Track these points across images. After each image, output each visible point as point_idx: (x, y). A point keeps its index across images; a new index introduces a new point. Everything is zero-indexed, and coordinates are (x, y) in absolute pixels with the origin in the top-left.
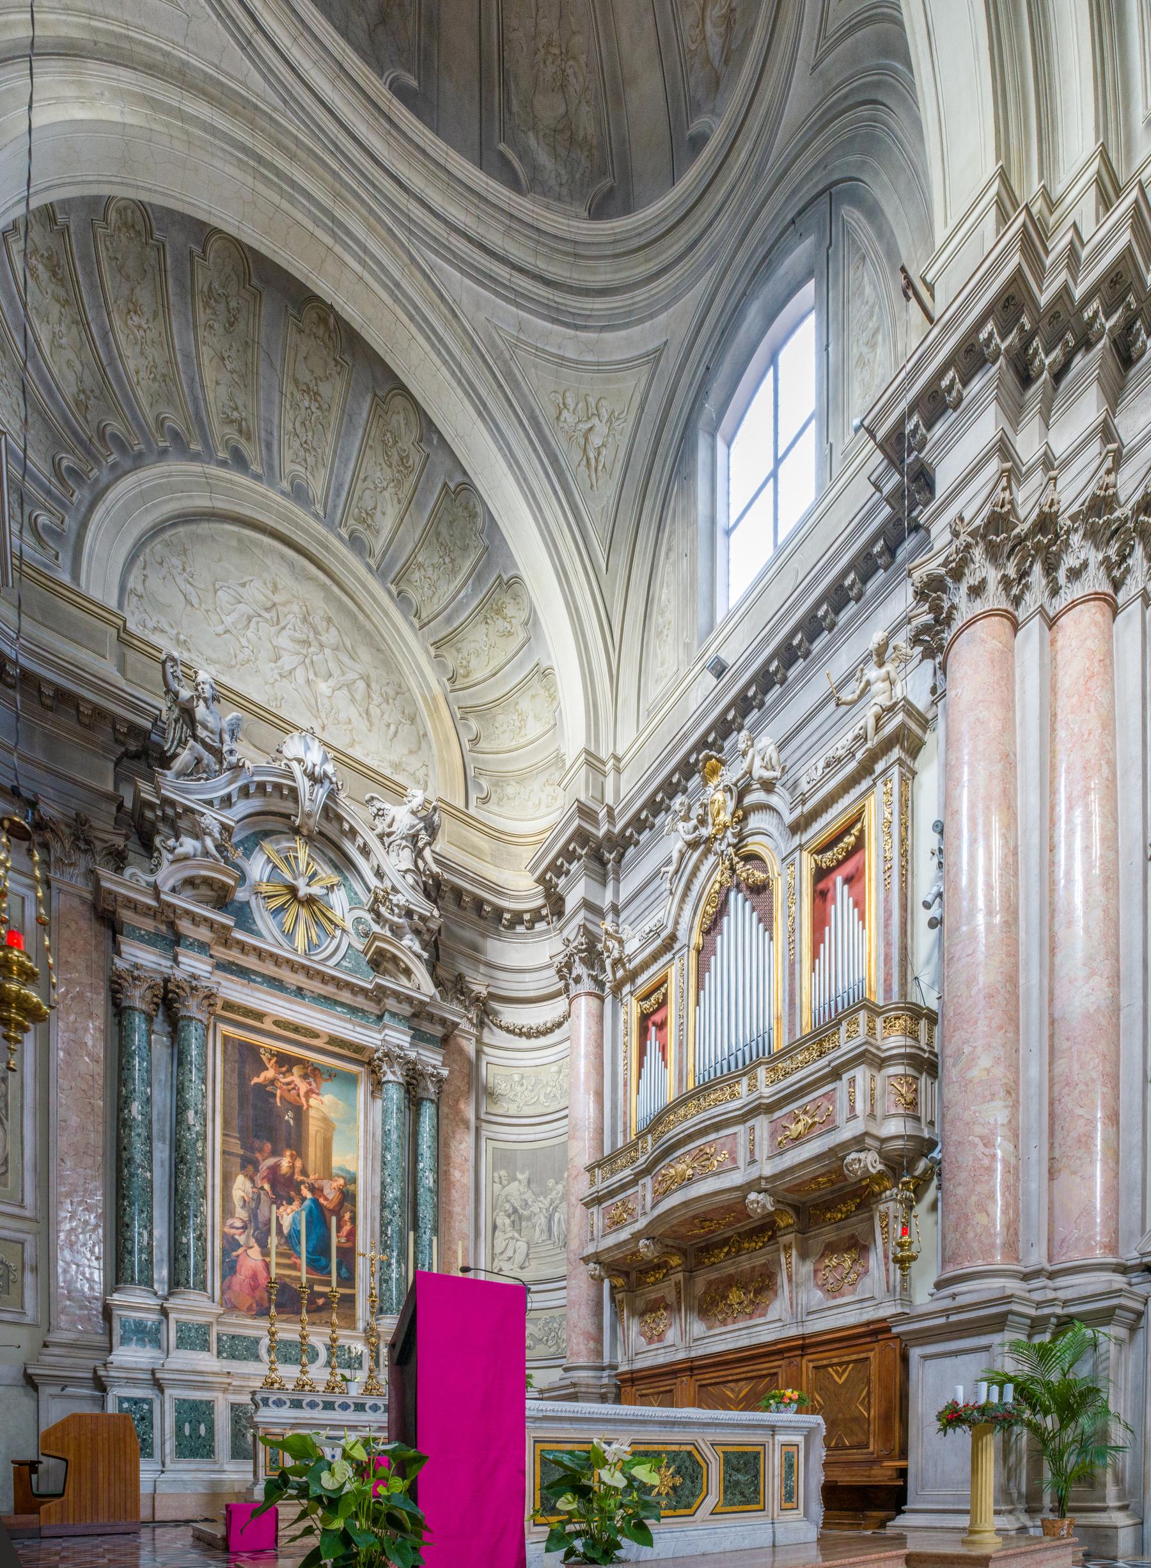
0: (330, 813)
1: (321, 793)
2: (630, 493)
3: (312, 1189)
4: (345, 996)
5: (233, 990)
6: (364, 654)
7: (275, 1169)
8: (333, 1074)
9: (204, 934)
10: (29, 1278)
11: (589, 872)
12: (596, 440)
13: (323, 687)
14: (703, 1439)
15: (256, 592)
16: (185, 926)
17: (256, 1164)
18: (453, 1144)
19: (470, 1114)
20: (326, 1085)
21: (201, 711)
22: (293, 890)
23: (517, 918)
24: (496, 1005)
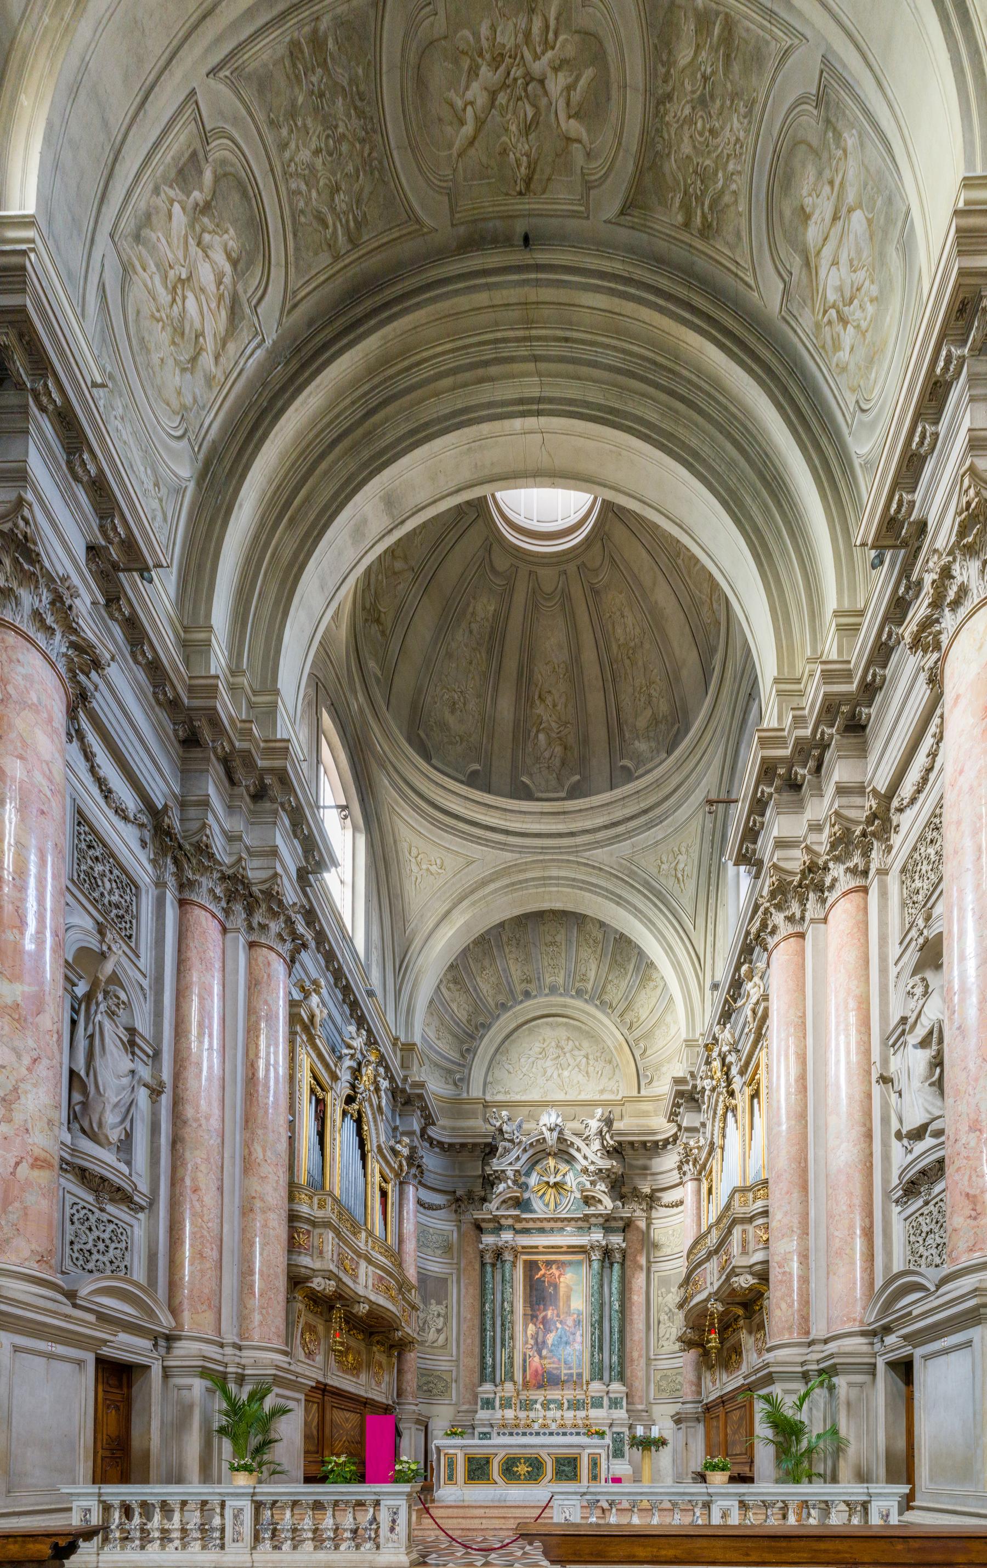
0: (561, 1140)
1: (555, 1134)
2: (703, 878)
5: (524, 1241)
6: (585, 1044)
7: (545, 1317)
8: (570, 1263)
9: (510, 1222)
10: (454, 1385)
11: (688, 1110)
12: (681, 866)
13: (566, 1073)
14: (543, 1454)
15: (537, 1047)
16: (503, 1221)
17: (537, 1317)
18: (634, 1281)
19: (643, 1261)
20: (567, 1269)
21: (505, 1128)
22: (548, 1183)
23: (666, 1142)
24: (659, 1194)
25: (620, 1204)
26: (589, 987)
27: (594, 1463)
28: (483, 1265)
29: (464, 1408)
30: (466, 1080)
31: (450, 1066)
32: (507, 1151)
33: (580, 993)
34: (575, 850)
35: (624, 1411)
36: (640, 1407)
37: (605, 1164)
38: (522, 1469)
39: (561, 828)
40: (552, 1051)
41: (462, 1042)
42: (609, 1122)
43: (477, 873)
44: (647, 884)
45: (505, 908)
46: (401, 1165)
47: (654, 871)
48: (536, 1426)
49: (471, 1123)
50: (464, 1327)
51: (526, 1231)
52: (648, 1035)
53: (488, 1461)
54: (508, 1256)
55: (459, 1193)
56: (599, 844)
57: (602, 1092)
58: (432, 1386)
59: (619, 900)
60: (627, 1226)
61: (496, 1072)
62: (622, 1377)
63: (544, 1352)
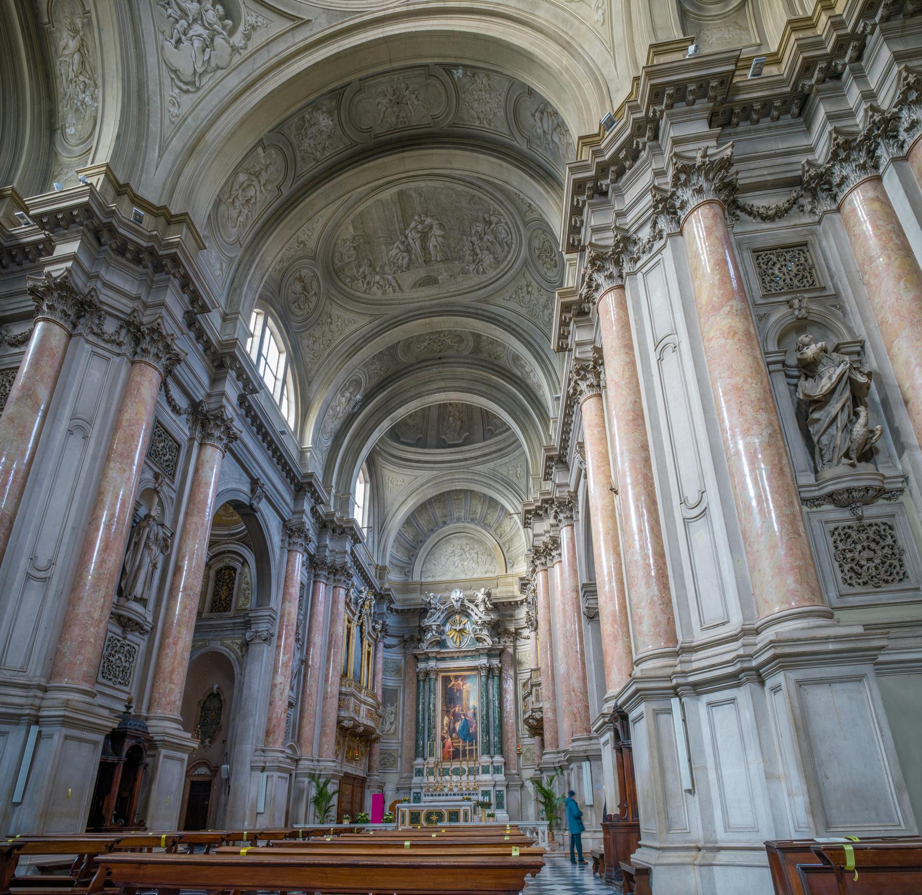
0: (463, 605)
1: (459, 603)
3: (464, 715)
4: (470, 654)
5: (442, 665)
6: (476, 546)
7: (454, 712)
9: (434, 655)
13: (466, 563)
15: (450, 550)
16: (430, 655)
19: (512, 673)
25: (496, 639)
26: (478, 517)
27: (466, 814)
28: (418, 681)
29: (405, 775)
30: (411, 572)
31: (402, 565)
32: (433, 614)
33: (473, 520)
34: (467, 467)
35: (502, 775)
36: (514, 772)
37: (487, 618)
38: (434, 818)
39: (460, 457)
40: (458, 551)
41: (409, 551)
42: (488, 595)
43: (419, 482)
44: (503, 480)
45: (433, 492)
46: (377, 636)
47: (506, 474)
48: (446, 790)
49: (413, 596)
50: (406, 720)
51: (443, 659)
52: (511, 540)
53: (419, 814)
54: (433, 676)
55: (406, 637)
56: (479, 464)
57: (486, 572)
58: (387, 761)
59: (489, 486)
60: (501, 653)
61: (428, 566)
62: (501, 752)
63: (454, 735)
